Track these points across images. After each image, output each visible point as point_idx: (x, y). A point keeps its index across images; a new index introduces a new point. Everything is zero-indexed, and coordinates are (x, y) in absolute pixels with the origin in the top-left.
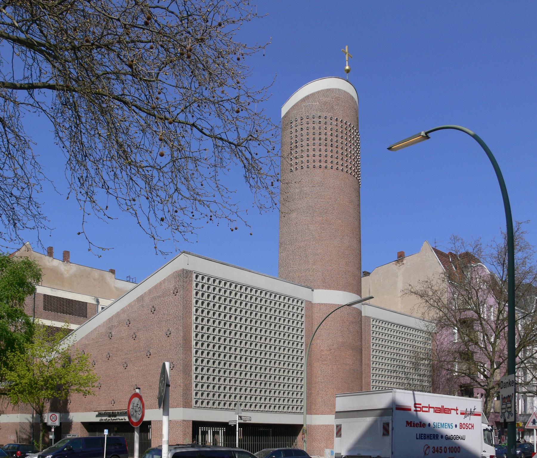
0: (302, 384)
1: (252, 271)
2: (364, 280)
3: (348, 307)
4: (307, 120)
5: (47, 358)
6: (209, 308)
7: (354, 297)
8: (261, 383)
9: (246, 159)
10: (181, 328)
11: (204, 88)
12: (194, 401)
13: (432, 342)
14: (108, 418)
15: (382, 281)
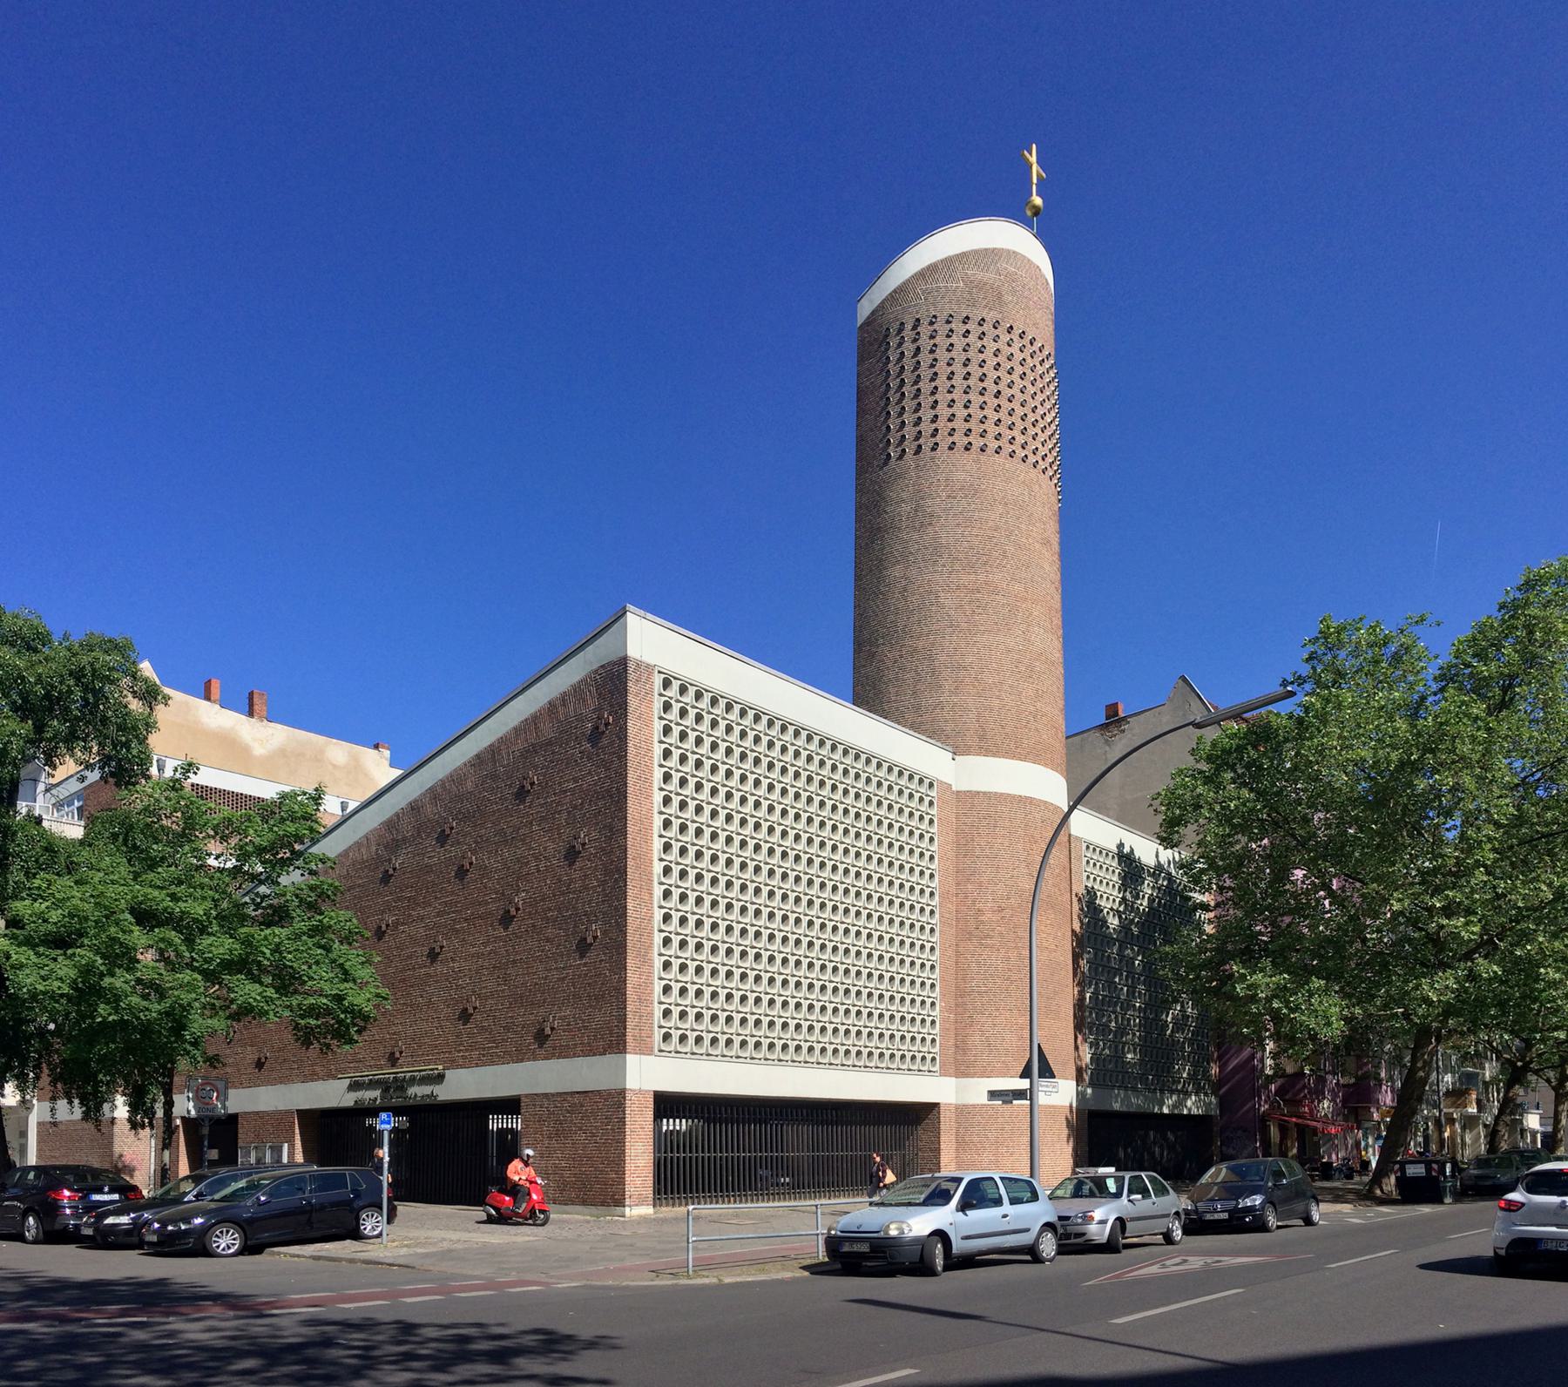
12: (658, 1035)
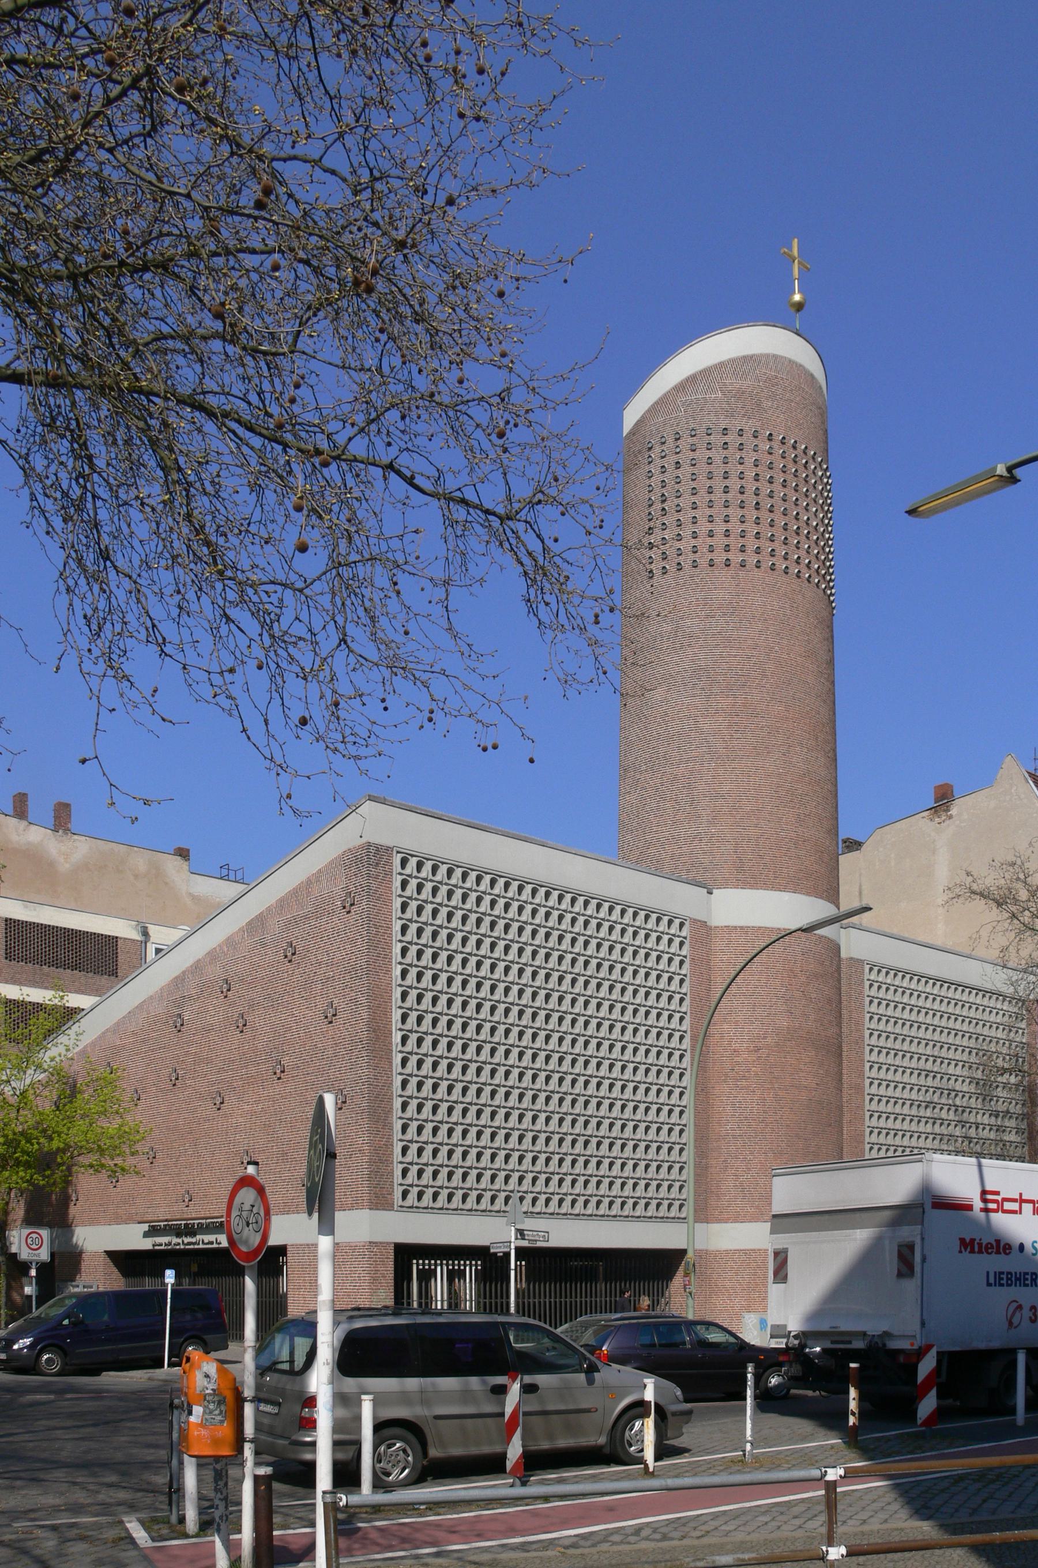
0: (684, 1141)
1: (550, 843)
2: (846, 861)
3: (804, 934)
4: (690, 440)
5: (13, 1084)
6: (438, 944)
7: (821, 909)
8: (574, 1142)
9: (530, 554)
10: (363, 1000)
11: (415, 370)
13: (1029, 1025)
14: (175, 1240)
15: (893, 864)
